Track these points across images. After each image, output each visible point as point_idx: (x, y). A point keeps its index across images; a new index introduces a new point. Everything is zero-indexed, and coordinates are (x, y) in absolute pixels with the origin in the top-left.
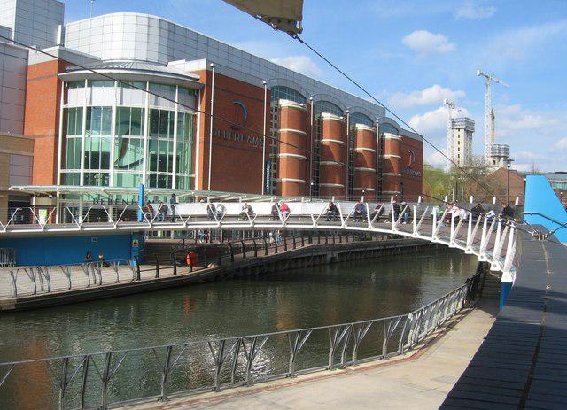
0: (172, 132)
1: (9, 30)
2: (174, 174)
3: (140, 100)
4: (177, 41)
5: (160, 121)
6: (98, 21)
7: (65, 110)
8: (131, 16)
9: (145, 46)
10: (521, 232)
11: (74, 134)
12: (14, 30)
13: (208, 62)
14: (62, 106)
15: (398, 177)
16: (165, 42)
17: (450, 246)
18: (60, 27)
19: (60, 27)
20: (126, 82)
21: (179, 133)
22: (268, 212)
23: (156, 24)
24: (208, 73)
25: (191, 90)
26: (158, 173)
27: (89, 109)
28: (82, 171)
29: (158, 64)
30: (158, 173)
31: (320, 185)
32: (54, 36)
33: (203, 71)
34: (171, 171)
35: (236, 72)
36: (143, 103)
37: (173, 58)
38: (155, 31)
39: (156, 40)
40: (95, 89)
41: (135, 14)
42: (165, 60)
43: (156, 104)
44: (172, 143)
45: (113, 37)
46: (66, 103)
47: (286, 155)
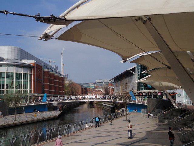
0: (22, 78)
2: (22, 89)
3: (13, 70)
4: (23, 54)
8: (10, 47)
9: (17, 56)
10: (99, 121)
11: (2, 81)
13: (35, 61)
15: (48, 78)
16: (19, 54)
20: (9, 65)
21: (24, 78)
22: (74, 98)
23: (17, 49)
24: (35, 63)
26: (25, 90)
29: (17, 60)
30: (25, 90)
34: (21, 89)
36: (14, 71)
41: (11, 46)
43: (17, 71)
44: (22, 81)
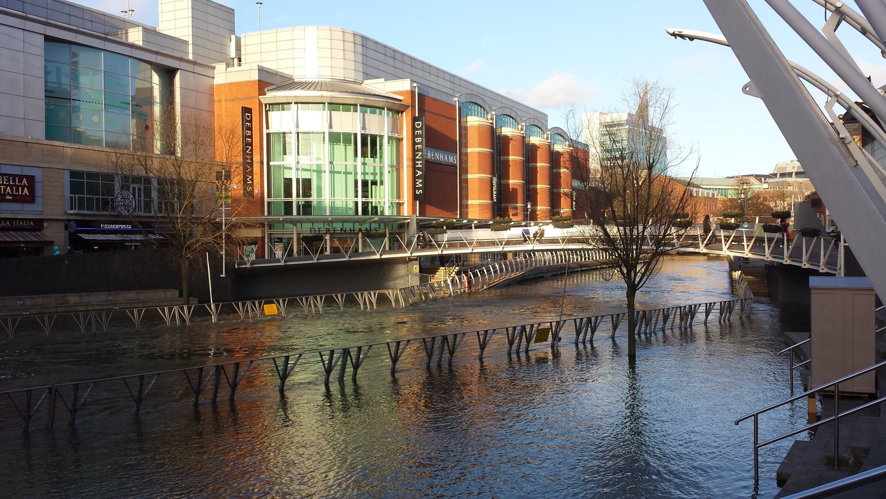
1: (186, 42)
5: (369, 145)
6: (285, 34)
7: (268, 135)
8: (311, 32)
12: (190, 42)
13: (412, 81)
14: (265, 131)
16: (360, 58)
17: (803, 267)
18: (233, 37)
19: (233, 37)
25: (396, 108)
27: (364, 137)
28: (101, 197)
29: (354, 82)
31: (503, 205)
32: (225, 46)
33: (407, 91)
35: (437, 90)
37: (367, 76)
38: (350, 46)
39: (351, 56)
40: (43, 102)
42: (360, 77)
45: (310, 53)
46: (268, 128)
47: (477, 176)
